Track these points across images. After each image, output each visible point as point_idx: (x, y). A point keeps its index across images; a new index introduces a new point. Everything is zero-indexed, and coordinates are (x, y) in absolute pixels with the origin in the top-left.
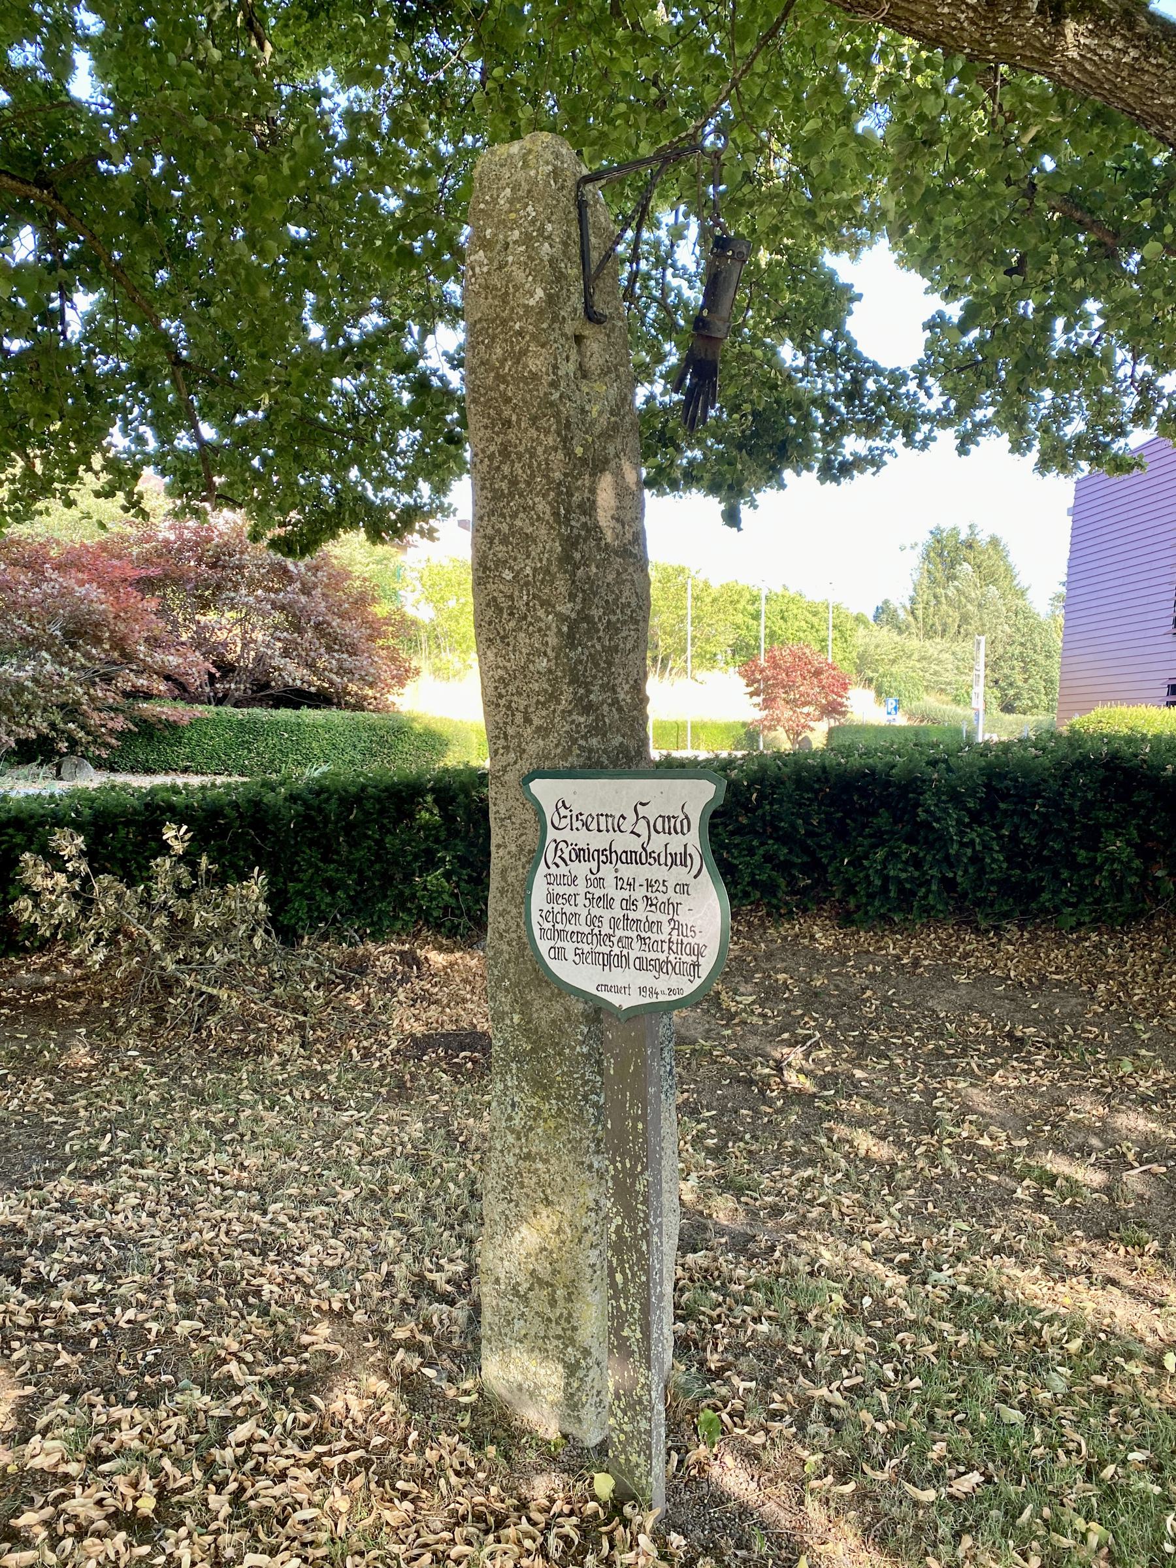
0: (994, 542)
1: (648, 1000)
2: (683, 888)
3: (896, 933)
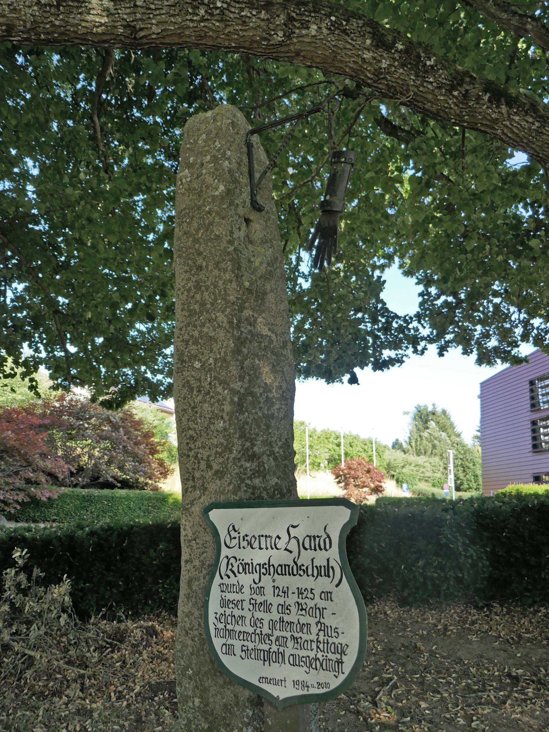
0: (444, 412)
1: (300, 692)
2: (327, 595)
3: (432, 610)
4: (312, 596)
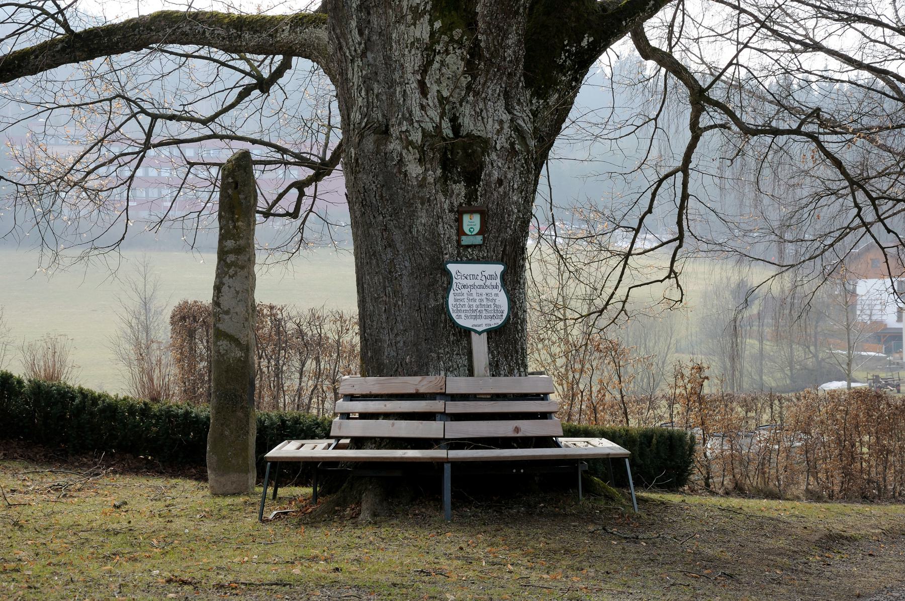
2: (496, 295)
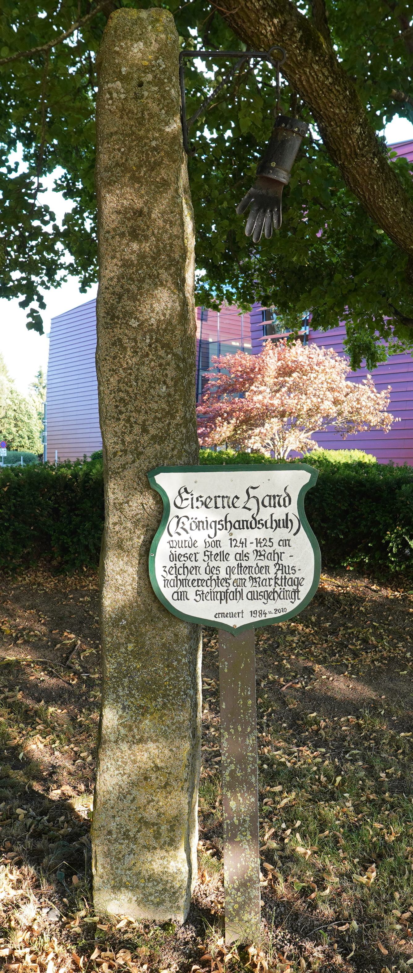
1: (258, 619)
2: (286, 542)
4: (271, 544)
